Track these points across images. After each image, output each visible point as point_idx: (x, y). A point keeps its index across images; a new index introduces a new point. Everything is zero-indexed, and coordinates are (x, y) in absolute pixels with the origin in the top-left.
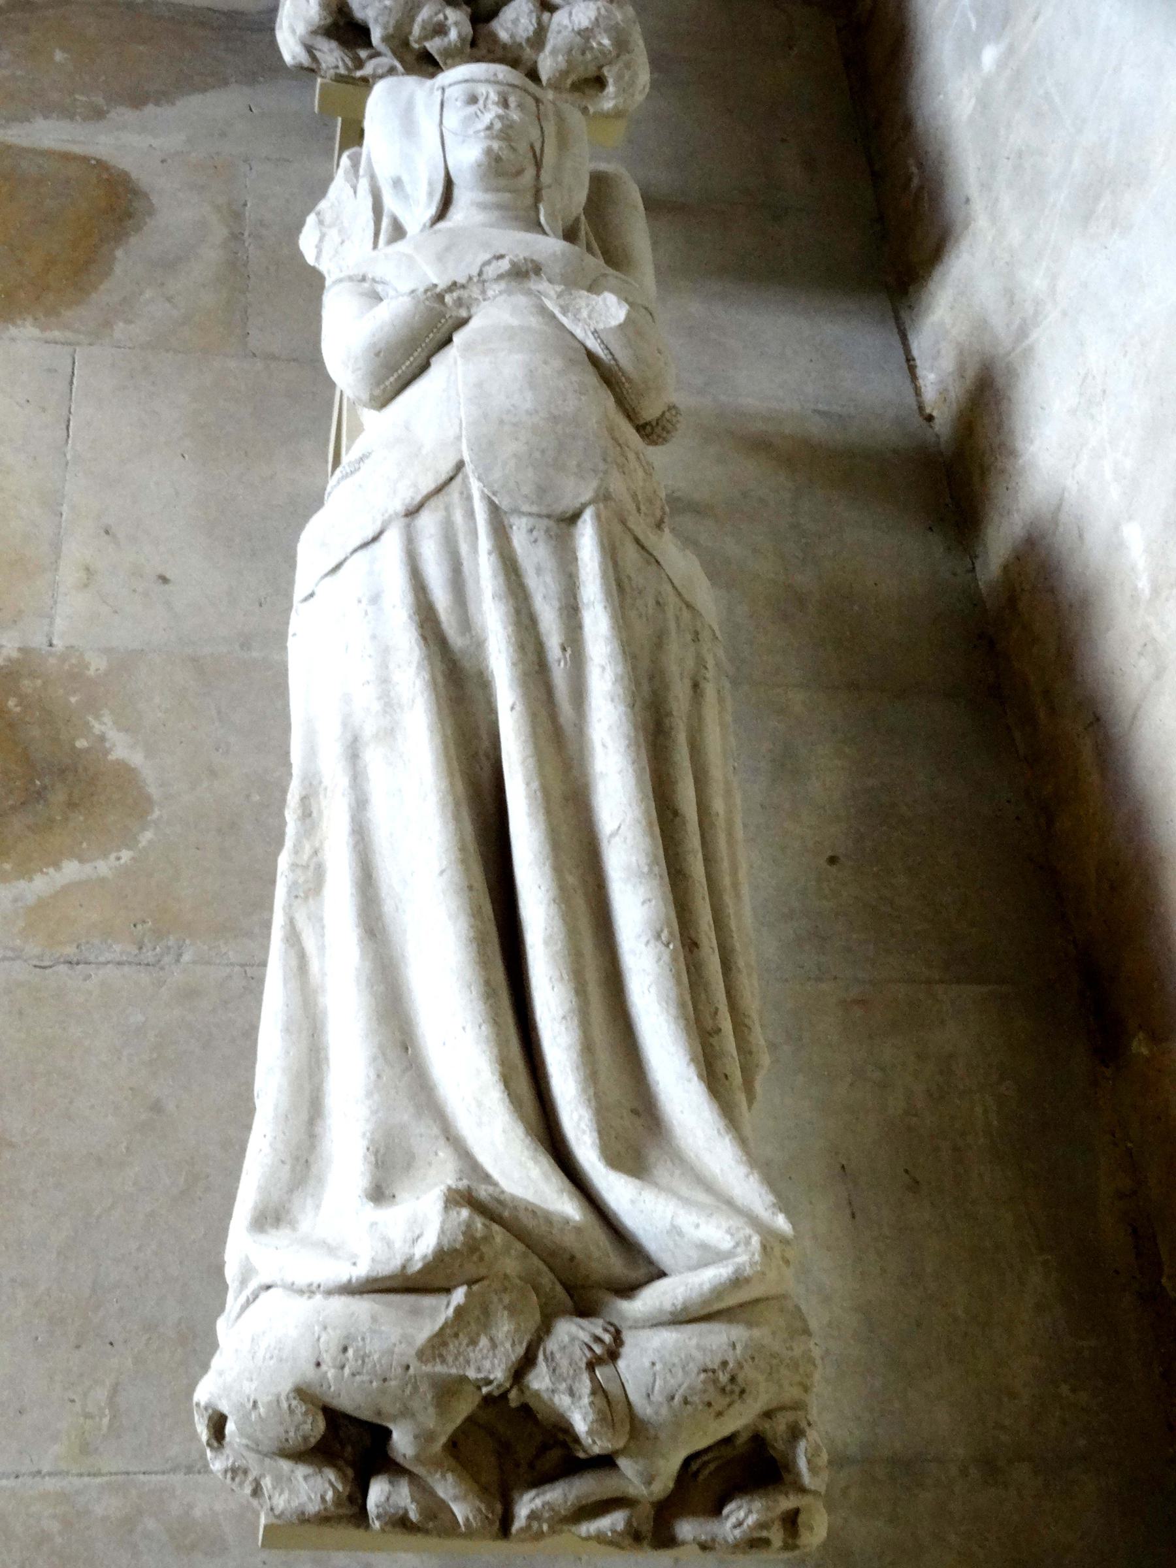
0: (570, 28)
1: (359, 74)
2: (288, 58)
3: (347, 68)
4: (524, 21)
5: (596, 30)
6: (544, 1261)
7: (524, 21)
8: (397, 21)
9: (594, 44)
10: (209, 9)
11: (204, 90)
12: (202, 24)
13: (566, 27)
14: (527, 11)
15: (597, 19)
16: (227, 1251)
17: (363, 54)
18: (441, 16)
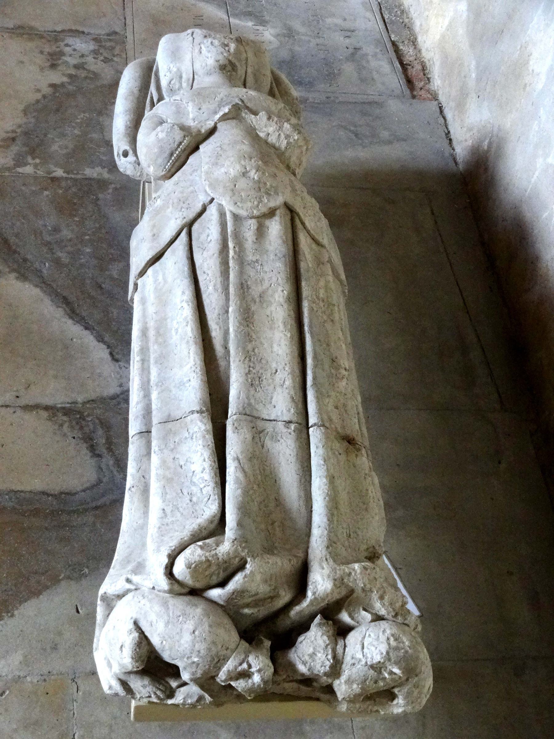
0: (363, 662)
1: (170, 702)
2: (105, 688)
3: (158, 697)
4: (320, 656)
5: (388, 664)
7: (320, 656)
8: (204, 671)
9: (386, 675)
10: (43, 493)
11: (37, 594)
12: (36, 513)
13: (360, 660)
14: (323, 645)
15: (388, 653)
16: (97, 668)
17: (174, 684)
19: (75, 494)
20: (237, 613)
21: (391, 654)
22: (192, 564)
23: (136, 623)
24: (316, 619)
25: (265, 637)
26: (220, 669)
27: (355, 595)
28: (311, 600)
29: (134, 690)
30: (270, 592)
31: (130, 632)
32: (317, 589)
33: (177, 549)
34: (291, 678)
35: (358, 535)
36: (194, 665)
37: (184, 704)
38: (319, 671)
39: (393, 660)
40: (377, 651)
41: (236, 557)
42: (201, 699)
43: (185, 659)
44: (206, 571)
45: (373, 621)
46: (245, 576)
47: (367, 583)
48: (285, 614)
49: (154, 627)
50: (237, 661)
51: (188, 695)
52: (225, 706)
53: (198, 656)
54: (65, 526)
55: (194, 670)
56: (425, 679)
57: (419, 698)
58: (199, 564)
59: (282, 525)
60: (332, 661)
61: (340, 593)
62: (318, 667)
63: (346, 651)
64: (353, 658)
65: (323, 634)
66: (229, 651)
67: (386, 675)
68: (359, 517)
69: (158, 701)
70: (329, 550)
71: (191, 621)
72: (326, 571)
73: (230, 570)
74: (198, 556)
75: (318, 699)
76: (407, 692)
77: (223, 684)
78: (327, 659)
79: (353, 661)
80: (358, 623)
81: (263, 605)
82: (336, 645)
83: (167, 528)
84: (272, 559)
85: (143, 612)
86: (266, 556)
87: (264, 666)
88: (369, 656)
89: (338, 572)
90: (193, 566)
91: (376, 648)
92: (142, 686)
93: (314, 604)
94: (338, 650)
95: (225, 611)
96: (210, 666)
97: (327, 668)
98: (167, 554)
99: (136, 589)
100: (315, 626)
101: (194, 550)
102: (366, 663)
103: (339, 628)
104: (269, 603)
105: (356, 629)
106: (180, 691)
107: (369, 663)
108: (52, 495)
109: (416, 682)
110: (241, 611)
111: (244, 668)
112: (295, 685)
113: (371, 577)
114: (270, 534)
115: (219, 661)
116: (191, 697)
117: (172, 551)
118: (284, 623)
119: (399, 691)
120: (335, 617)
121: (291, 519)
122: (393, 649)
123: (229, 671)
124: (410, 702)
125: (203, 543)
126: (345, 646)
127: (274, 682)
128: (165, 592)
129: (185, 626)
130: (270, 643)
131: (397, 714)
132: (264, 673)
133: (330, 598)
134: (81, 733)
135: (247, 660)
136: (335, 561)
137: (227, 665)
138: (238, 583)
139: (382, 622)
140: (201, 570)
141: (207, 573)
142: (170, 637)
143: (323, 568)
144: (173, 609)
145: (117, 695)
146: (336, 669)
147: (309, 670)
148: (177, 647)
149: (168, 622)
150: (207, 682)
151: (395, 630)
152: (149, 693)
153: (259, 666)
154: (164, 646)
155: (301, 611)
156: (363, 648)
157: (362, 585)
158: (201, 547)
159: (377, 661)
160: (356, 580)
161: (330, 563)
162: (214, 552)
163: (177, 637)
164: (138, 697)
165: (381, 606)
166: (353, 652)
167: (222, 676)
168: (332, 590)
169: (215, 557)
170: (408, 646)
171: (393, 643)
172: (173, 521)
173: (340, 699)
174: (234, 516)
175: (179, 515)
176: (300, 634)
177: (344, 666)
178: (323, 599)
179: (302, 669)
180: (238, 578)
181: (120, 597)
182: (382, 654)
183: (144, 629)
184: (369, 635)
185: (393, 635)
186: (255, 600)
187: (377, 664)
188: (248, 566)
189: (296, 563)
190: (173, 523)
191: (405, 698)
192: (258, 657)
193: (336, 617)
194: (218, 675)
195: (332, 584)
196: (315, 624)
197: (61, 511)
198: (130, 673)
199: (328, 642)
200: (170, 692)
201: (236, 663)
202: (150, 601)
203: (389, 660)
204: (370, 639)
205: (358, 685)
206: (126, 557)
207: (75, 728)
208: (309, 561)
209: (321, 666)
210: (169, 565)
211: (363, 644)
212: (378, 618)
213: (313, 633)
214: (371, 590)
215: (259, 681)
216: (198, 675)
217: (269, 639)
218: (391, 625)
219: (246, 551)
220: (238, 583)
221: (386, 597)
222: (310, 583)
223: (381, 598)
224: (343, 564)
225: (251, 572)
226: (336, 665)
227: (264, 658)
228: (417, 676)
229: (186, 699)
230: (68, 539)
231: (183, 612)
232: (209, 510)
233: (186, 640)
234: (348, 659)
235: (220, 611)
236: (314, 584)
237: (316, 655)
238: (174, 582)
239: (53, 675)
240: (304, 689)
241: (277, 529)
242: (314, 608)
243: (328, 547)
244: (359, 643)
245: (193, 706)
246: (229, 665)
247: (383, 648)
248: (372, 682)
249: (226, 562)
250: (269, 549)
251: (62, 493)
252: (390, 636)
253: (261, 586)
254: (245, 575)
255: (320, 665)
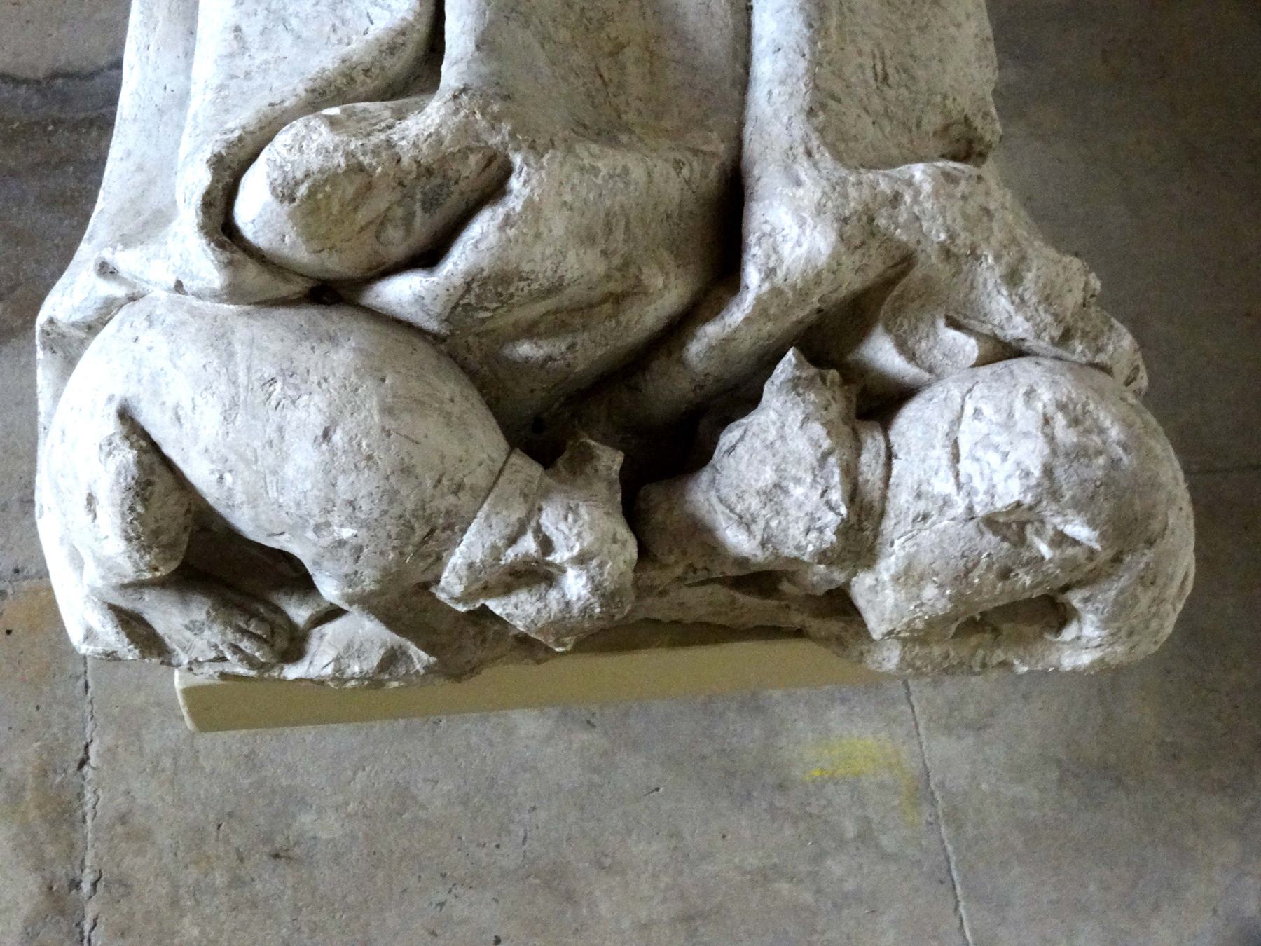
1: (292, 672)
2: (75, 635)
3: (250, 661)
4: (802, 493)
5: (1048, 509)
6: (483, 503)
7: (802, 493)
8: (385, 571)
9: (1045, 550)
13: (946, 502)
15: (1048, 471)
18: (528, 544)
19: (90, 76)
20: (494, 358)
21: (1059, 473)
22: (297, 184)
23: (126, 416)
24: (780, 367)
25: (605, 440)
26: (439, 560)
27: (917, 273)
28: (758, 299)
29: (167, 640)
30: (608, 277)
31: (109, 448)
32: (780, 261)
33: (249, 139)
34: (702, 575)
35: (913, 78)
36: (345, 552)
37: (340, 677)
38: (798, 548)
39: (1068, 495)
40: (1009, 465)
41: (466, 151)
42: (392, 659)
43: (310, 534)
44: (356, 209)
45: (983, 361)
46: (507, 222)
47: (957, 228)
48: (670, 354)
49: (187, 426)
50: (496, 530)
51: (349, 646)
52: (487, 672)
53: (351, 520)
54: (63, 162)
55: (348, 568)
56: (1172, 554)
57: (1155, 615)
58: (324, 182)
59: (651, 56)
60: (843, 510)
61: (860, 270)
62: (796, 531)
63: (894, 472)
64: (919, 496)
65: (807, 418)
66: (465, 497)
67: (1045, 550)
68: (913, 25)
69: (253, 673)
70: (815, 121)
71: (317, 398)
72: (810, 192)
73: (452, 204)
74: (318, 151)
75: (799, 633)
76: (1116, 602)
77: (461, 608)
78: (828, 503)
79: (921, 506)
80: (930, 370)
81: (585, 327)
82: (858, 450)
83: (246, 84)
84: (607, 161)
85: (145, 372)
86: (587, 152)
87: (601, 540)
88: (980, 485)
89: (853, 192)
90: (303, 190)
91: (1006, 455)
92: (187, 627)
93: (772, 311)
94: (864, 469)
95: (452, 356)
96: (402, 554)
97: (830, 536)
98: (208, 155)
99: (132, 299)
100: (780, 390)
101: (303, 132)
102: (970, 509)
103: (865, 394)
104: (610, 317)
105: (926, 394)
106: (322, 637)
107: (979, 511)
108: (26, 81)
109: (1147, 565)
110: (507, 351)
111: (526, 554)
112: (722, 594)
113: (972, 208)
114: (605, 84)
115: (432, 531)
116: (360, 655)
117: (230, 145)
118: (668, 388)
119: (1086, 600)
120: (847, 353)
121: (681, 36)
122: (1067, 455)
123: (471, 566)
124: (1123, 633)
125: (343, 111)
126: (890, 456)
127: (642, 590)
128: (216, 296)
129: (294, 416)
130: (619, 458)
131: (1075, 672)
132: (601, 565)
133: (825, 288)
134: (109, 740)
135: (533, 524)
136: (838, 157)
137: (462, 547)
138: (483, 246)
139: (1017, 365)
140: (335, 208)
141: (362, 216)
142: (242, 457)
143: (798, 183)
144: (250, 358)
145: (111, 657)
146: (861, 534)
147: (763, 545)
148: (273, 494)
149: (234, 404)
150: (405, 603)
151: (1068, 388)
152: (216, 646)
153: (580, 541)
154: (230, 489)
155: (727, 341)
156: (956, 458)
157: (943, 236)
158: (333, 123)
159: (1010, 500)
160: (918, 218)
161: (821, 165)
162: (383, 137)
163: (271, 459)
164: (185, 661)
165: (1011, 308)
166: (918, 474)
167: (451, 584)
168: (835, 257)
169: (384, 155)
170: (1119, 443)
171: (1065, 435)
172: (267, 62)
173: (876, 636)
174: (470, 21)
175: (287, 39)
176: (726, 421)
177: (888, 524)
178: (802, 294)
179: (738, 541)
180: (483, 230)
181: (92, 328)
182: (1028, 474)
183: (156, 435)
184: (977, 412)
185: (1062, 407)
186: (557, 311)
187: (1008, 513)
188: (515, 183)
189: (705, 174)
190: (265, 68)
191: (1105, 623)
192: (574, 510)
193: (850, 358)
194: (438, 582)
195: (833, 237)
196: (777, 382)
197: (55, 124)
198: (138, 586)
199: (826, 444)
200: (292, 640)
201: (495, 537)
202: (170, 333)
203: (1055, 495)
204: (982, 427)
205: (941, 586)
206: (132, 202)
207: (90, 726)
208: (745, 162)
209: (808, 531)
210: (219, 194)
211: (956, 445)
212: (1002, 351)
213: (773, 415)
214: (973, 252)
215: (585, 593)
216: (369, 583)
217: (616, 446)
218: (1051, 371)
219: (506, 127)
220: (483, 246)
221: (1030, 276)
222: (752, 239)
223: (1013, 278)
224: (871, 167)
225: (529, 203)
226: (860, 521)
227: (598, 513)
228: (1150, 543)
229: (345, 661)
230: (73, 197)
231: (286, 365)
232: (387, 14)
233: (303, 460)
234: (901, 500)
235: (424, 352)
236: (766, 243)
237: (786, 491)
238: (239, 256)
239: (26, 578)
240: (751, 605)
241: (632, 69)
242: (769, 327)
243: (811, 112)
244: (939, 439)
245: (373, 682)
246: (470, 548)
247: (1032, 453)
248: (991, 576)
249: (429, 172)
250: (606, 130)
251: (55, 76)
252: (1051, 409)
253: (571, 257)
254: (507, 216)
255: (802, 526)
